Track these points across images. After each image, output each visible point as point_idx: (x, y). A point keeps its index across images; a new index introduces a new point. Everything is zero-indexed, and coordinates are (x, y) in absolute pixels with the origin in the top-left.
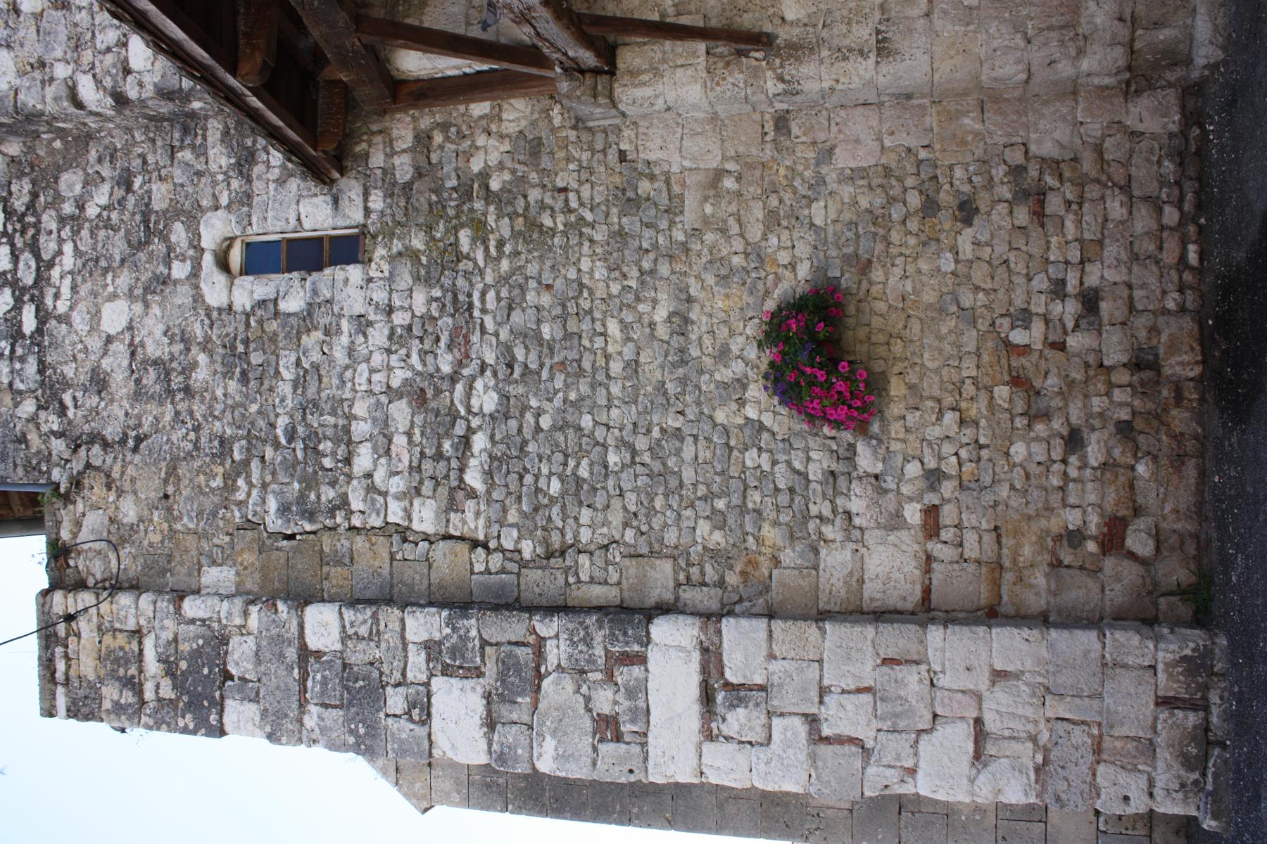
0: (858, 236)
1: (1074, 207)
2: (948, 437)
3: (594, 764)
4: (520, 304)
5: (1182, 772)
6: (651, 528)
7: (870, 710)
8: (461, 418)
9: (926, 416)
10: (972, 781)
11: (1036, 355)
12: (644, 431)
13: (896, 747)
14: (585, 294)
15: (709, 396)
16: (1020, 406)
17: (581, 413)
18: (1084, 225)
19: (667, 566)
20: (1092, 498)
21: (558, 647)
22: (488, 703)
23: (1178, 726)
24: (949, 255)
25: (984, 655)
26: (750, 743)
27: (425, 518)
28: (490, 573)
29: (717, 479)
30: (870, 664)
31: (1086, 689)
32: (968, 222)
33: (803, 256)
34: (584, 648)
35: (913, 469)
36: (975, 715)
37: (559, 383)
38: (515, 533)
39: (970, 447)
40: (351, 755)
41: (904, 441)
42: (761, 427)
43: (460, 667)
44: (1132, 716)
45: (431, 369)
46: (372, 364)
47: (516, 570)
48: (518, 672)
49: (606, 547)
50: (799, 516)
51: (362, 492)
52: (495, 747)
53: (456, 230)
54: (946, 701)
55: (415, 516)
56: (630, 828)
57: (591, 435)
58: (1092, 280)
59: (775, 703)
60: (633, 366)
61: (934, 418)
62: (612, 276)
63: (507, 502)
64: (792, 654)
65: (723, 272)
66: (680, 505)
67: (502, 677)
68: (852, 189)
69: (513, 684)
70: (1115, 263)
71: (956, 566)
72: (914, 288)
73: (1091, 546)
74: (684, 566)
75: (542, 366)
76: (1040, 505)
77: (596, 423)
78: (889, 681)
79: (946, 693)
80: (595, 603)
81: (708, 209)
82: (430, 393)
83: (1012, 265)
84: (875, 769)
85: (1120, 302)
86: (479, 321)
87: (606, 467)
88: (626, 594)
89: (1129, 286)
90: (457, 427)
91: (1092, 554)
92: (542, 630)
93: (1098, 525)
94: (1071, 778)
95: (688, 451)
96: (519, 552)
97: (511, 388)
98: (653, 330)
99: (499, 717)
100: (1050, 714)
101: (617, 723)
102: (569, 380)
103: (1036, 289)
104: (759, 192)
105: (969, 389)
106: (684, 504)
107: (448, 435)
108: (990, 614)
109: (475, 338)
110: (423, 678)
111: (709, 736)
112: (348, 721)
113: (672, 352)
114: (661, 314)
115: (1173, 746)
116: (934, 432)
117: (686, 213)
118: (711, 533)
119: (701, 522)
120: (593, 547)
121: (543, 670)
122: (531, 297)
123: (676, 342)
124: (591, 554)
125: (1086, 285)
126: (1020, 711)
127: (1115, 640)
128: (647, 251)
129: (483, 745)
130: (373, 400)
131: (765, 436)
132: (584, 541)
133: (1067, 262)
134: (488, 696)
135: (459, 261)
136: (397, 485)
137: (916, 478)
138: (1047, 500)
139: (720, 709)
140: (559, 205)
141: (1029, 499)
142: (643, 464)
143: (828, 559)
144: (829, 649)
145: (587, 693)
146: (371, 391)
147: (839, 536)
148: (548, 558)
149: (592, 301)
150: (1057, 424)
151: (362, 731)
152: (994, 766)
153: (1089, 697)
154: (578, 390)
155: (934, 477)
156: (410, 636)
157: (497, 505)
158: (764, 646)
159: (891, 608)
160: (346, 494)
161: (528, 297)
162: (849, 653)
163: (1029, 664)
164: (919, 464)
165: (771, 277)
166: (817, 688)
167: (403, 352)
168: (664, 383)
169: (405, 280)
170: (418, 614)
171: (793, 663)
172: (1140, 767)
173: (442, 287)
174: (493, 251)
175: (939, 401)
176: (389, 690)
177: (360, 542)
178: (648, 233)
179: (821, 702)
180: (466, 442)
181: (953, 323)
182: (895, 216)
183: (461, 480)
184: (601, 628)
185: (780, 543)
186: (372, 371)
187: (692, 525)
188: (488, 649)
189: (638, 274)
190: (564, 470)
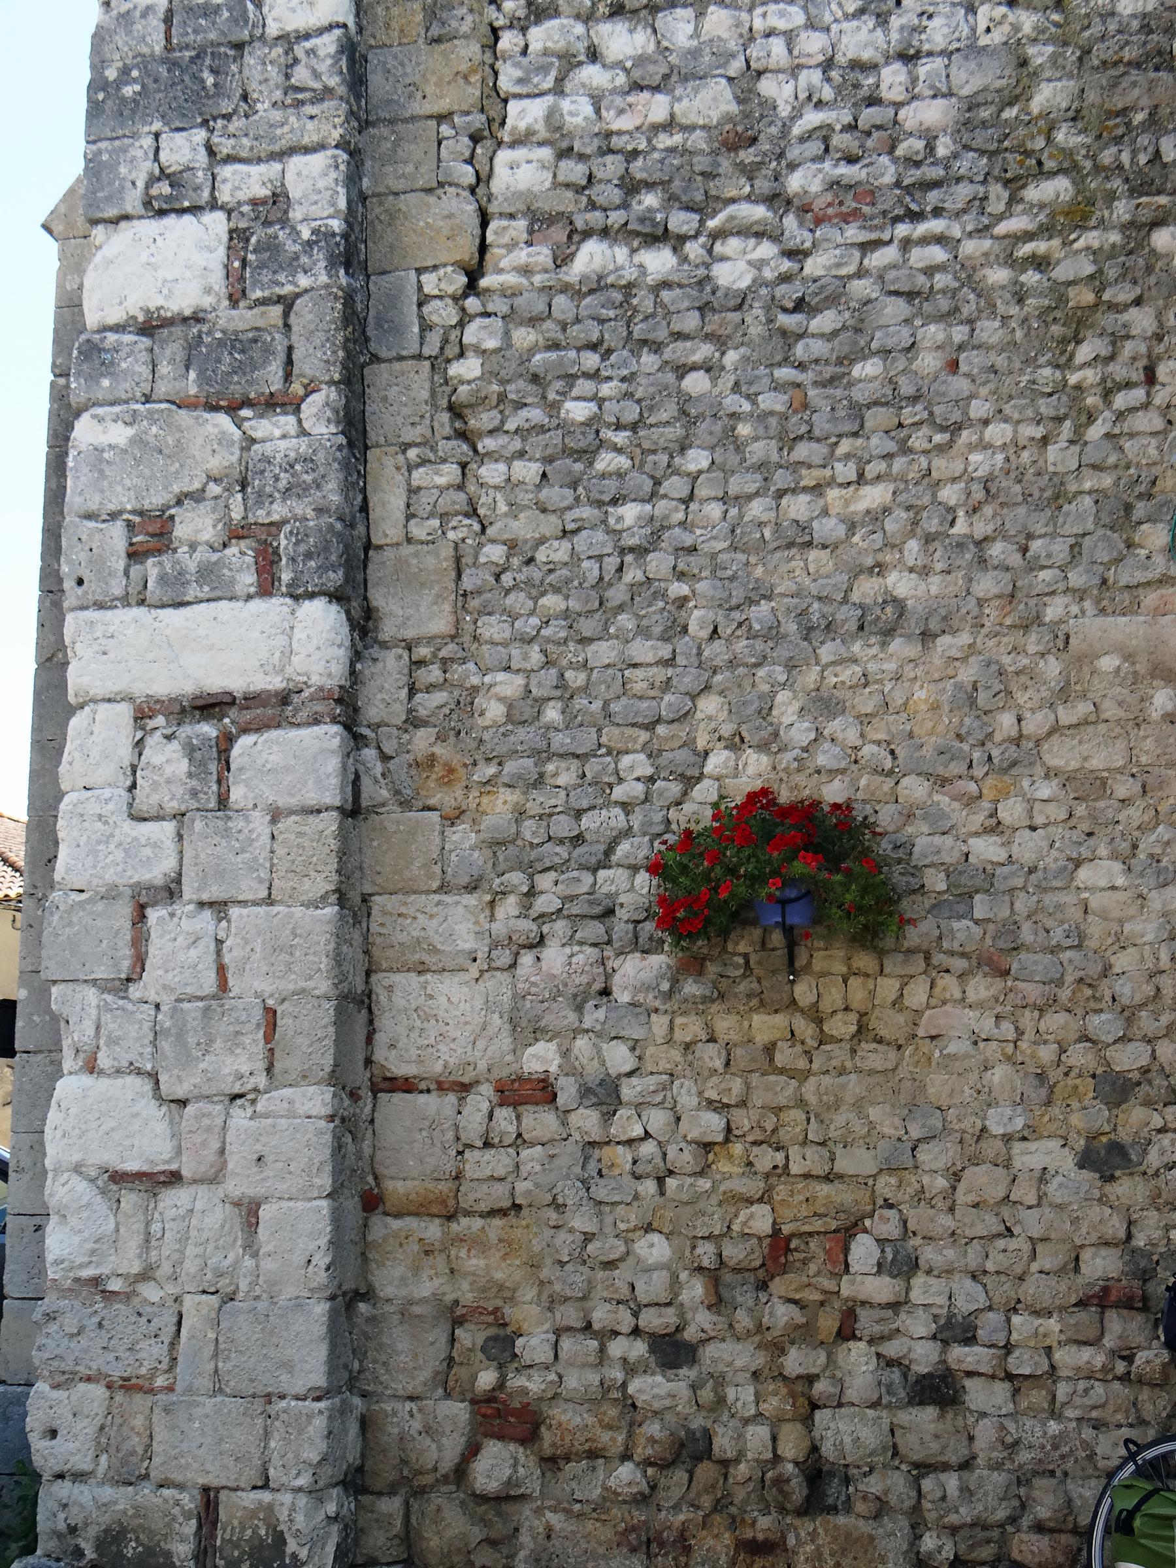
0: (1054, 950)
1: (1121, 1367)
2: (678, 1119)
3: (89, 516)
4: (920, 313)
5: (93, 1531)
6: (508, 592)
7: (188, 990)
8: (702, 222)
9: (715, 1080)
10: (77, 1169)
11: (828, 1284)
12: (681, 566)
13: (130, 1038)
14: (939, 438)
15: (747, 683)
16: (734, 1252)
17: (712, 448)
18: (1082, 1385)
19: (441, 624)
20: (572, 1382)
21: (284, 437)
22: (185, 320)
23: (168, 1525)
24: (1019, 1123)
25: (282, 1187)
26: (134, 786)
27: (520, 173)
28: (420, 305)
29: (597, 706)
30: (264, 986)
31: (229, 1366)
32: (1085, 1161)
33: (1015, 849)
34: (283, 484)
35: (619, 1058)
36: (185, 1173)
37: (770, 401)
38: (491, 344)
39: (658, 1160)
40: (86, 76)
41: (669, 1041)
42: (690, 781)
43: (244, 262)
44: (185, 1446)
45: (793, 153)
46: (803, 35)
47: (427, 351)
48: (239, 368)
49: (473, 513)
50: (534, 854)
51: (561, 45)
52: (112, 337)
53: (1070, 169)
54: (206, 1122)
55: (520, 153)
56: (37, 593)
57: (672, 470)
58: (978, 1394)
59: (198, 825)
60: (801, 539)
61: (712, 1094)
62: (975, 487)
63: (549, 325)
64: (281, 851)
65: (982, 697)
66: (548, 640)
67: (233, 341)
68: (1149, 937)
69: (219, 361)
70: (1009, 1440)
71: (450, 1135)
72: (953, 1057)
73: (487, 1379)
74: (443, 653)
75: (801, 366)
76: (557, 1287)
77: (695, 477)
78: (238, 1022)
79: (219, 1121)
80: (373, 500)
81: (1108, 663)
82: (747, 156)
83: (1001, 1243)
84: (94, 1002)
85: (935, 1446)
86: (886, 236)
87: (614, 502)
88: (389, 553)
89: (966, 1465)
90: (683, 216)
91: (474, 1377)
92: (310, 407)
93: (525, 1391)
94: (84, 1341)
95: (644, 650)
96: (462, 355)
97: (758, 311)
98: (870, 570)
99: (164, 341)
100: (189, 1302)
101: (160, 552)
102: (773, 421)
103: (955, 1286)
104: (1144, 759)
105: (766, 1159)
106: (550, 648)
107: (671, 199)
108: (361, 1195)
109: (853, 233)
110: (225, 196)
111: (141, 717)
112: (144, 62)
113: (828, 609)
114: (900, 584)
115: (137, 1515)
116: (686, 1096)
117: (1100, 620)
118: (501, 700)
119: (520, 680)
120: (472, 488)
121: (245, 413)
122: (934, 332)
123: (847, 616)
124: (461, 487)
125: (968, 1383)
126: (191, 1251)
127: (310, 1417)
128: (1024, 550)
129: (115, 316)
130: (733, 45)
131: (675, 788)
132: (483, 471)
133: (1008, 1348)
134: (197, 318)
135: (1007, 183)
136: (577, 111)
137: (603, 1063)
138: (567, 1299)
139: (186, 730)
140: (1118, 370)
141: (569, 1268)
142: (620, 569)
143: (460, 909)
144: (290, 916)
145: (209, 494)
146: (752, 39)
147: (499, 928)
148: (451, 408)
149: (926, 452)
150: (702, 1320)
151: (128, 91)
152: (101, 1206)
153: (216, 1371)
154: (756, 439)
155: (605, 1095)
156: (296, 162)
157: (541, 306)
158: (293, 802)
159: (376, 1023)
160: (557, 14)
161: (932, 328)
162: (286, 950)
163: (268, 1265)
164: (627, 1068)
165: (972, 787)
166: (223, 896)
167: (827, 93)
168: (768, 598)
169: (969, 79)
170: (333, 175)
171: (265, 853)
172: (104, 1458)
173: (955, 156)
174: (1027, 249)
175: (743, 1104)
176: (200, 135)
177: (469, 51)
178: (1060, 549)
179: (201, 905)
180: (658, 236)
181: (887, 1130)
182: (1095, 1020)
183: (587, 234)
184: (319, 511)
185: (487, 822)
186: (790, 37)
187: (514, 666)
188: (277, 311)
189: (978, 536)
190: (609, 425)
